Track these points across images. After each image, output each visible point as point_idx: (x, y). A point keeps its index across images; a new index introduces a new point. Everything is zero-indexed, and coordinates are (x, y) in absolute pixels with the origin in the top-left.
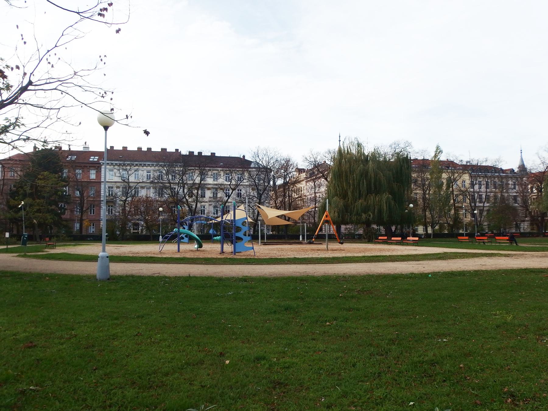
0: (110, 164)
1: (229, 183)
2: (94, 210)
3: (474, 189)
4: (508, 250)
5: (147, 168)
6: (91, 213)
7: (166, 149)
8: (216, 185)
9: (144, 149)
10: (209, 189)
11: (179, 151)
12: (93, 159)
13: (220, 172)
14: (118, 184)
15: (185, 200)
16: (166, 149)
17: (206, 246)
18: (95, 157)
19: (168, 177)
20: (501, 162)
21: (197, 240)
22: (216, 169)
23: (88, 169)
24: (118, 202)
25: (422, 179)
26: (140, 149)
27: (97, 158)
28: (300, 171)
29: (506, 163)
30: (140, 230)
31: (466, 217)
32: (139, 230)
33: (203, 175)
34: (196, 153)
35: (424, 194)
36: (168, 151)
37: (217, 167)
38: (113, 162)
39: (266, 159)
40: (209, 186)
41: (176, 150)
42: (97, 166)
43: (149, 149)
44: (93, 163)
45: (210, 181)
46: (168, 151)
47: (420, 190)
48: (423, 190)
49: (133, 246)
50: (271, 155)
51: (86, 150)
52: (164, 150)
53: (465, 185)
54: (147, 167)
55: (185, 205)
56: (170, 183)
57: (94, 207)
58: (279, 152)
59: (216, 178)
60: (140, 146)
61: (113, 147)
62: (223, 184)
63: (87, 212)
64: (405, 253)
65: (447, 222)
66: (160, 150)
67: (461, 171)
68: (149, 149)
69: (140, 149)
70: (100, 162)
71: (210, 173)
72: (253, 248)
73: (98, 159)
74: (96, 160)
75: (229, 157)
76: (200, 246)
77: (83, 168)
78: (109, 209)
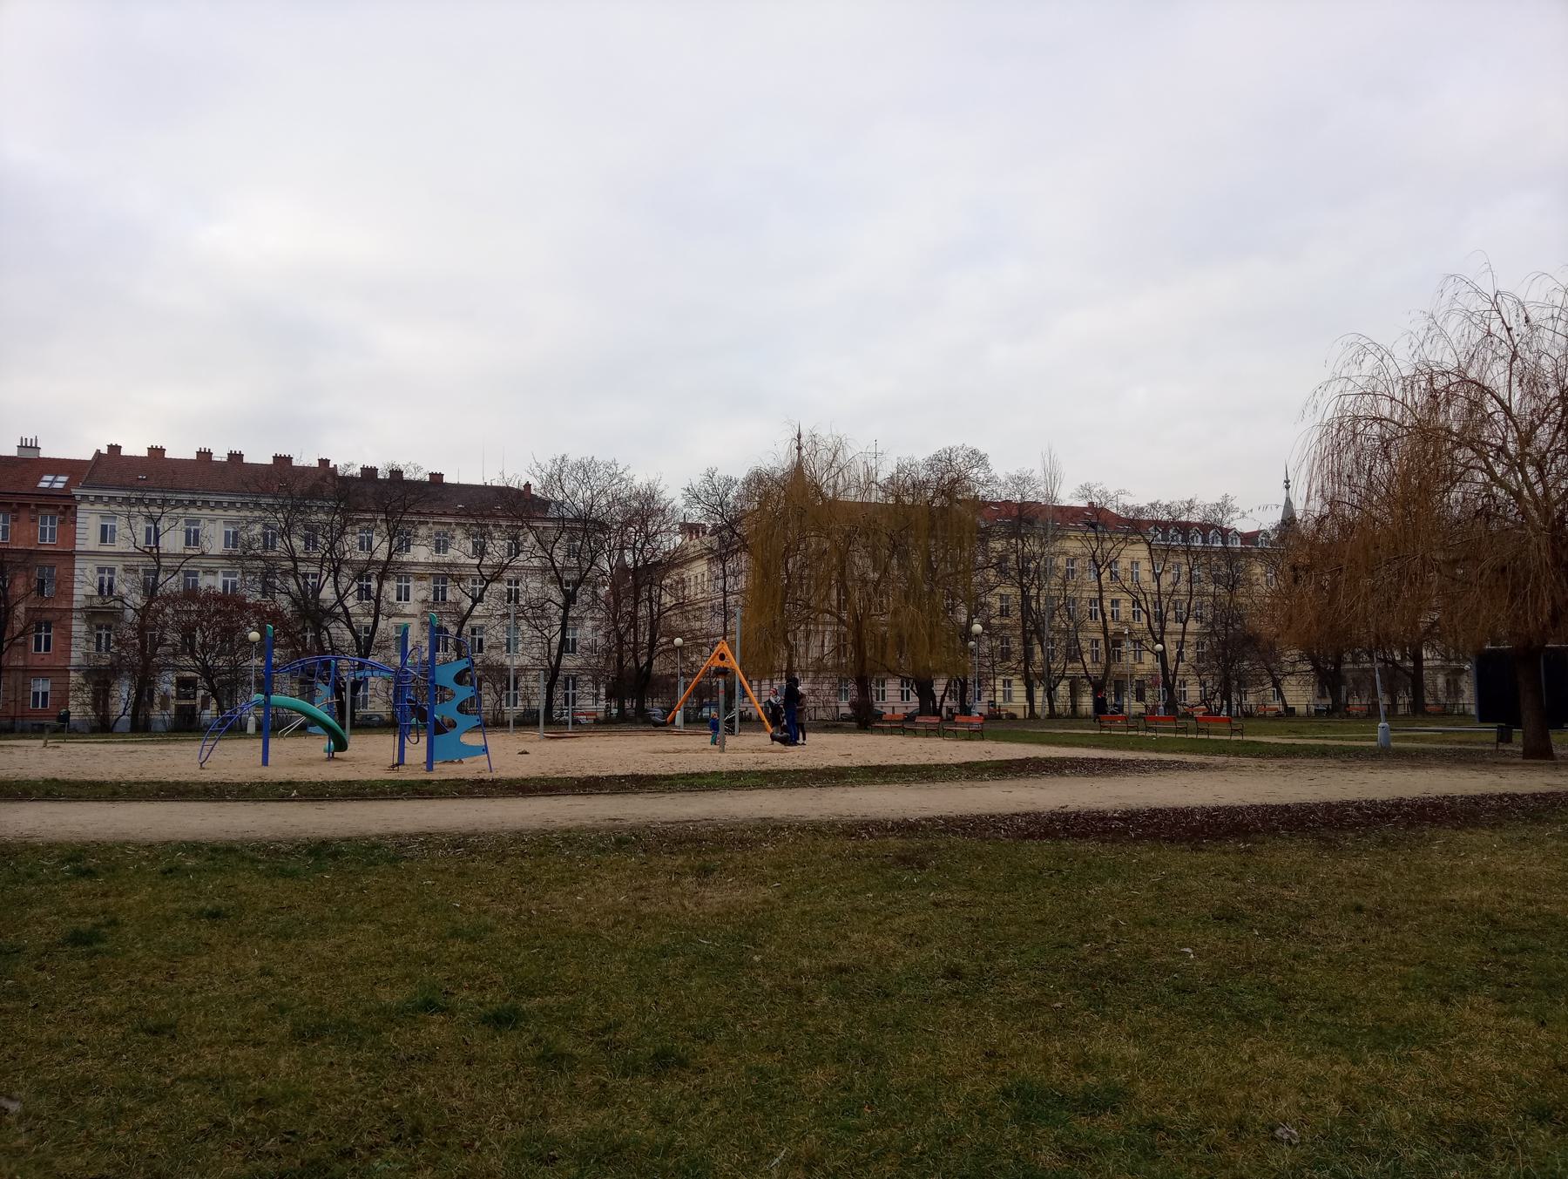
0: (238, 505)
1: (477, 561)
2: (48, 639)
3: (1159, 585)
4: (1174, 752)
5: (92, 507)
6: (38, 648)
7: (162, 450)
8: (437, 565)
9: (220, 455)
10: (420, 578)
11: (331, 466)
12: (52, 482)
13: (454, 531)
14: (133, 561)
15: (339, 610)
16: (162, 450)
17: (281, 747)
18: (56, 476)
19: (287, 542)
20: (1229, 511)
21: (328, 729)
22: (444, 520)
23: (33, 512)
24: (129, 613)
25: (1018, 557)
26: (205, 456)
27: (65, 479)
28: (690, 529)
29: (1244, 515)
30: (199, 700)
31: (1140, 663)
32: (195, 698)
33: (401, 538)
34: (104, 451)
35: (1026, 598)
36: (167, 455)
37: (445, 514)
38: (169, 496)
39: (584, 494)
40: (415, 570)
41: (110, 447)
42: (63, 506)
43: (235, 457)
44: (50, 494)
45: (420, 553)
46: (167, 455)
47: (1013, 585)
48: (1022, 585)
49: (131, 747)
50: (597, 486)
51: (30, 454)
52: (282, 461)
53: (1137, 573)
54: (225, 509)
55: (342, 625)
56: (293, 558)
57: (48, 630)
58: (624, 476)
59: (441, 547)
60: (205, 445)
61: (327, 461)
62: (456, 565)
63: (25, 644)
64: (945, 758)
65: (1086, 672)
66: (145, 453)
67: (1122, 536)
68: (235, 457)
69: (205, 456)
70: (74, 491)
71: (423, 531)
72: (485, 750)
73: (66, 483)
74: (60, 485)
75: (65, 460)
76: (341, 745)
77: (14, 511)
78: (99, 636)
